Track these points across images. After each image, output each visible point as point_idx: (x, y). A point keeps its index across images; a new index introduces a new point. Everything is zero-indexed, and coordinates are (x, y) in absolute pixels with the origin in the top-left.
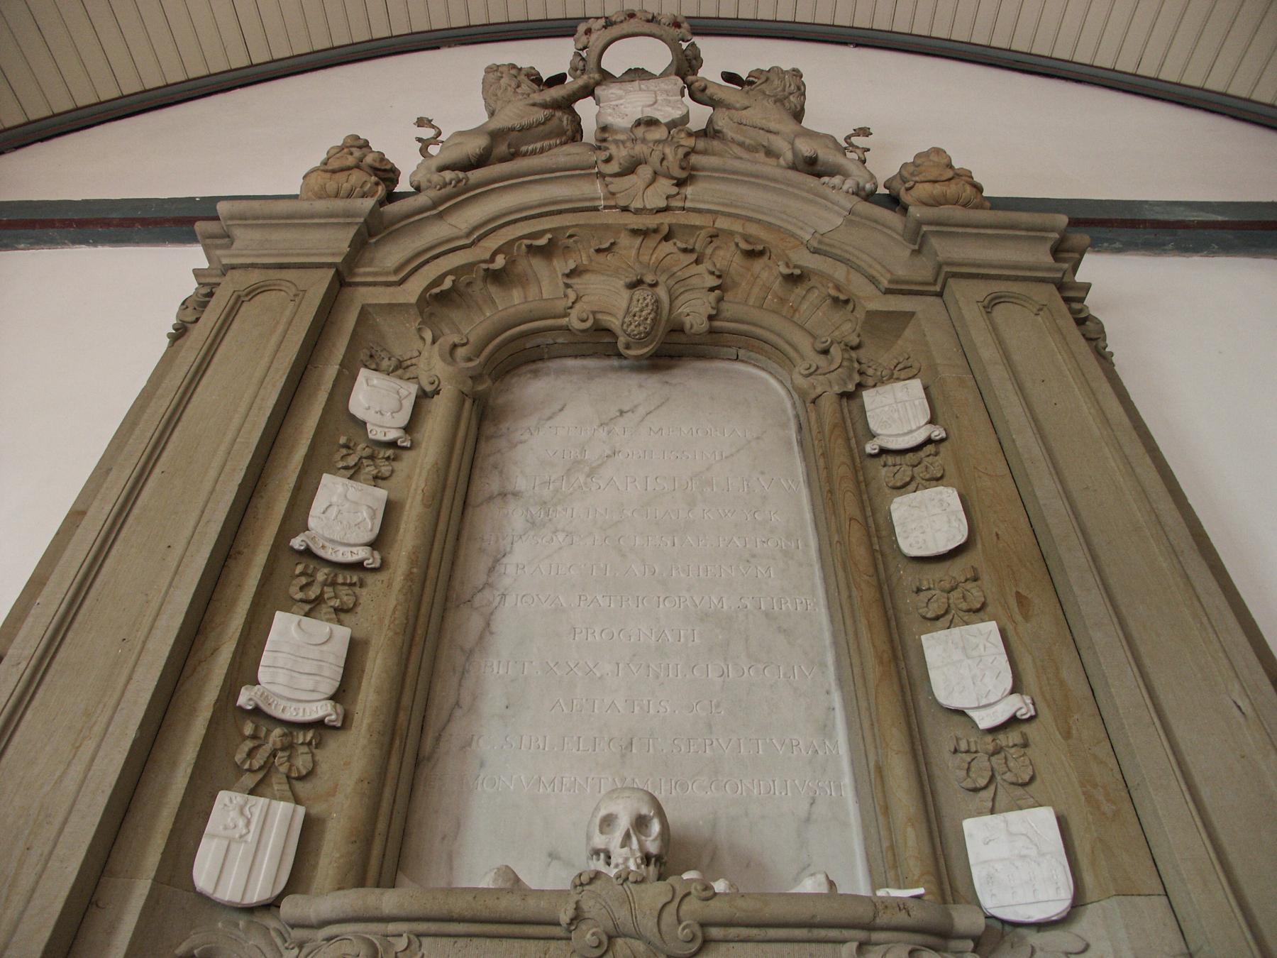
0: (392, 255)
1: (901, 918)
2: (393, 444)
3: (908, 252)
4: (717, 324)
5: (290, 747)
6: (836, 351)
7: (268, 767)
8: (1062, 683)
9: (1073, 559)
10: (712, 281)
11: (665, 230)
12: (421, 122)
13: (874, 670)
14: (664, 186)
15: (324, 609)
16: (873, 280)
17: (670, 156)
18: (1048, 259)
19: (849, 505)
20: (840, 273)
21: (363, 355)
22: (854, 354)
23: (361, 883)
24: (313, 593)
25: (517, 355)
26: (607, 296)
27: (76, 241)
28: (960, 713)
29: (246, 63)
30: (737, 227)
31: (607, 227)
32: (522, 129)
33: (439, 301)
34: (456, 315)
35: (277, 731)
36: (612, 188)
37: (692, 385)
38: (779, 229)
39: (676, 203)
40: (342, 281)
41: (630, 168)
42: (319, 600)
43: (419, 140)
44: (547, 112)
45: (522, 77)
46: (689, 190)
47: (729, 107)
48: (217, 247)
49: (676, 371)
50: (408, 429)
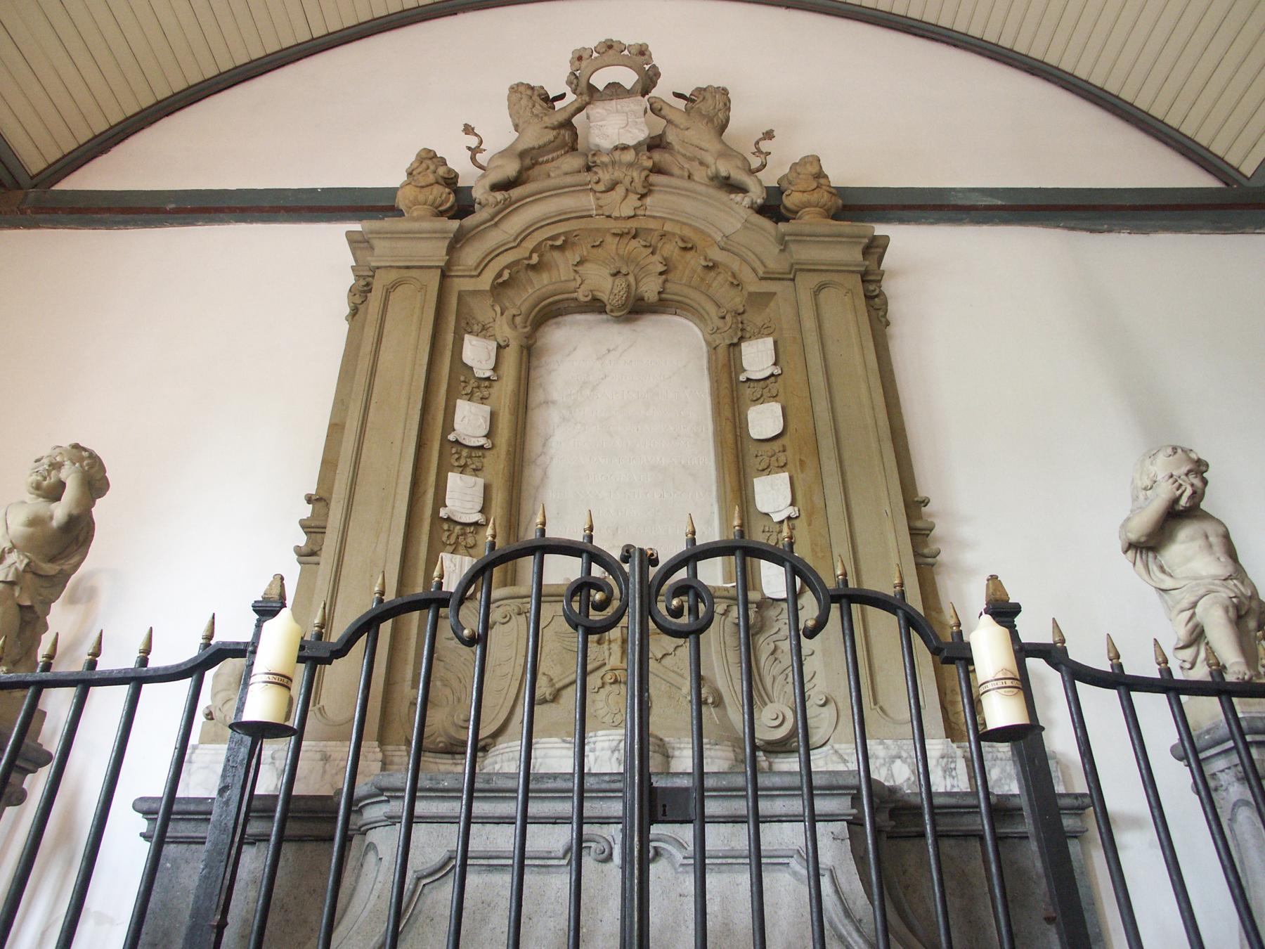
0: (471, 255)
1: (725, 594)
2: (488, 379)
3: (777, 251)
4: (664, 296)
5: (464, 534)
6: (728, 318)
7: (457, 543)
8: (812, 502)
9: (827, 443)
10: (661, 268)
11: (633, 232)
12: (468, 130)
13: (730, 495)
14: (633, 200)
15: (468, 470)
16: (754, 270)
17: (636, 179)
18: (860, 257)
19: (727, 412)
20: (735, 265)
21: (463, 325)
22: (739, 318)
23: (505, 585)
24: (462, 462)
25: (549, 312)
26: (599, 280)
27: (238, 221)
28: (767, 514)
29: (308, 37)
30: (677, 230)
31: (598, 230)
32: (540, 147)
33: (500, 287)
34: (511, 293)
35: (458, 527)
36: (601, 202)
37: (653, 329)
38: (702, 232)
39: (640, 212)
40: (445, 274)
41: (612, 188)
42: (465, 466)
43: (469, 148)
44: (555, 133)
45: (535, 98)
46: (648, 200)
47: (676, 126)
48: (361, 249)
49: (640, 323)
50: (494, 369)
